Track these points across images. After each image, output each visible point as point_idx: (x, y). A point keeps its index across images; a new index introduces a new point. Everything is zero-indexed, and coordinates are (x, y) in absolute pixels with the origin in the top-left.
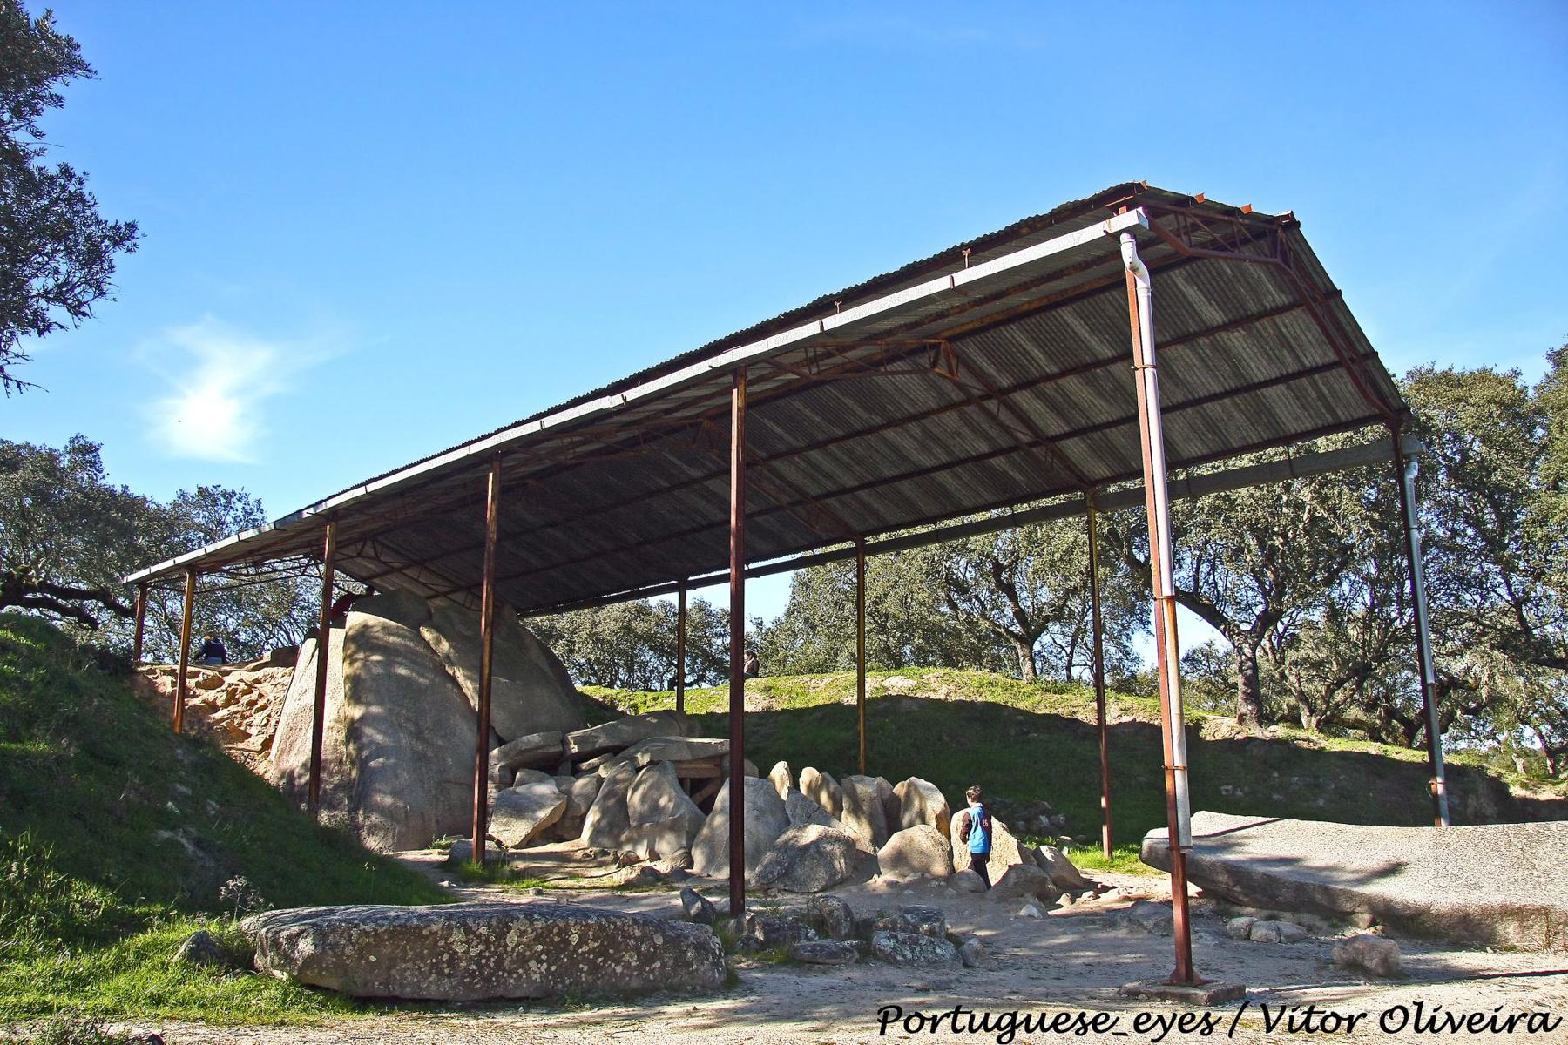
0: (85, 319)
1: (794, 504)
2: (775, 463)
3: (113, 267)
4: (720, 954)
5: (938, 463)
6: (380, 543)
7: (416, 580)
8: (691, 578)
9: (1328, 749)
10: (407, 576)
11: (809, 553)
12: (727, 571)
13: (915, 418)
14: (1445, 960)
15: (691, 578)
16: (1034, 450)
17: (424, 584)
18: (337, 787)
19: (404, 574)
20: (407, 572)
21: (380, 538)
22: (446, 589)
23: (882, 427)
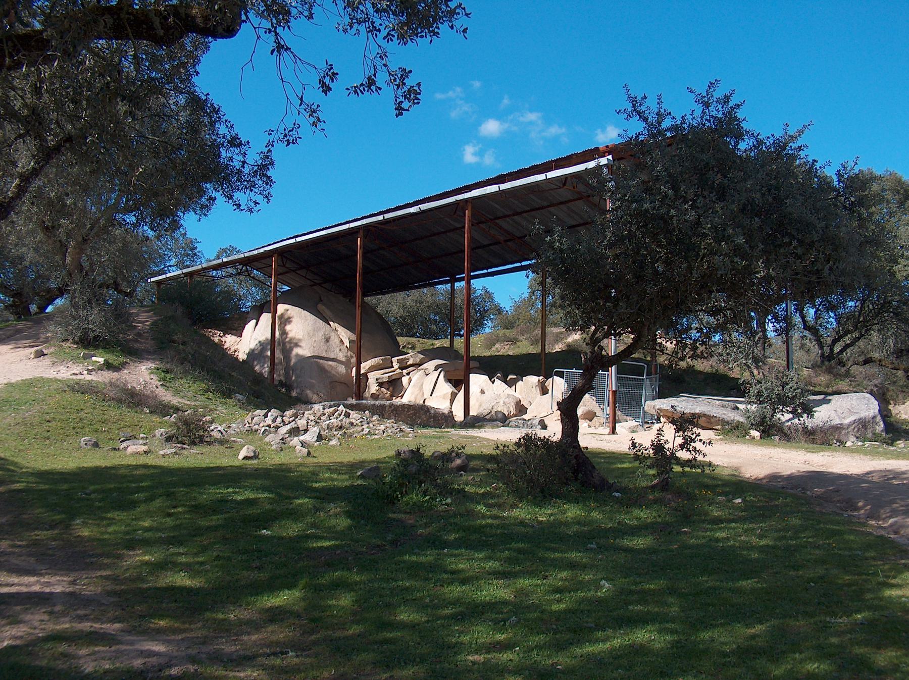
0: (221, 109)
1: (506, 241)
2: (497, 221)
3: (335, 74)
4: (249, 609)
5: (578, 223)
6: (284, 256)
7: (305, 277)
8: (457, 277)
9: (428, 452)
10: (501, 228)
11: (519, 264)
12: (464, 275)
13: (562, 203)
14: (297, 656)
15: (457, 277)
16: (509, 243)
17: (309, 279)
18: (749, 271)
19: (297, 273)
20: (298, 272)
21: (285, 254)
22: (321, 282)
23: (548, 206)
